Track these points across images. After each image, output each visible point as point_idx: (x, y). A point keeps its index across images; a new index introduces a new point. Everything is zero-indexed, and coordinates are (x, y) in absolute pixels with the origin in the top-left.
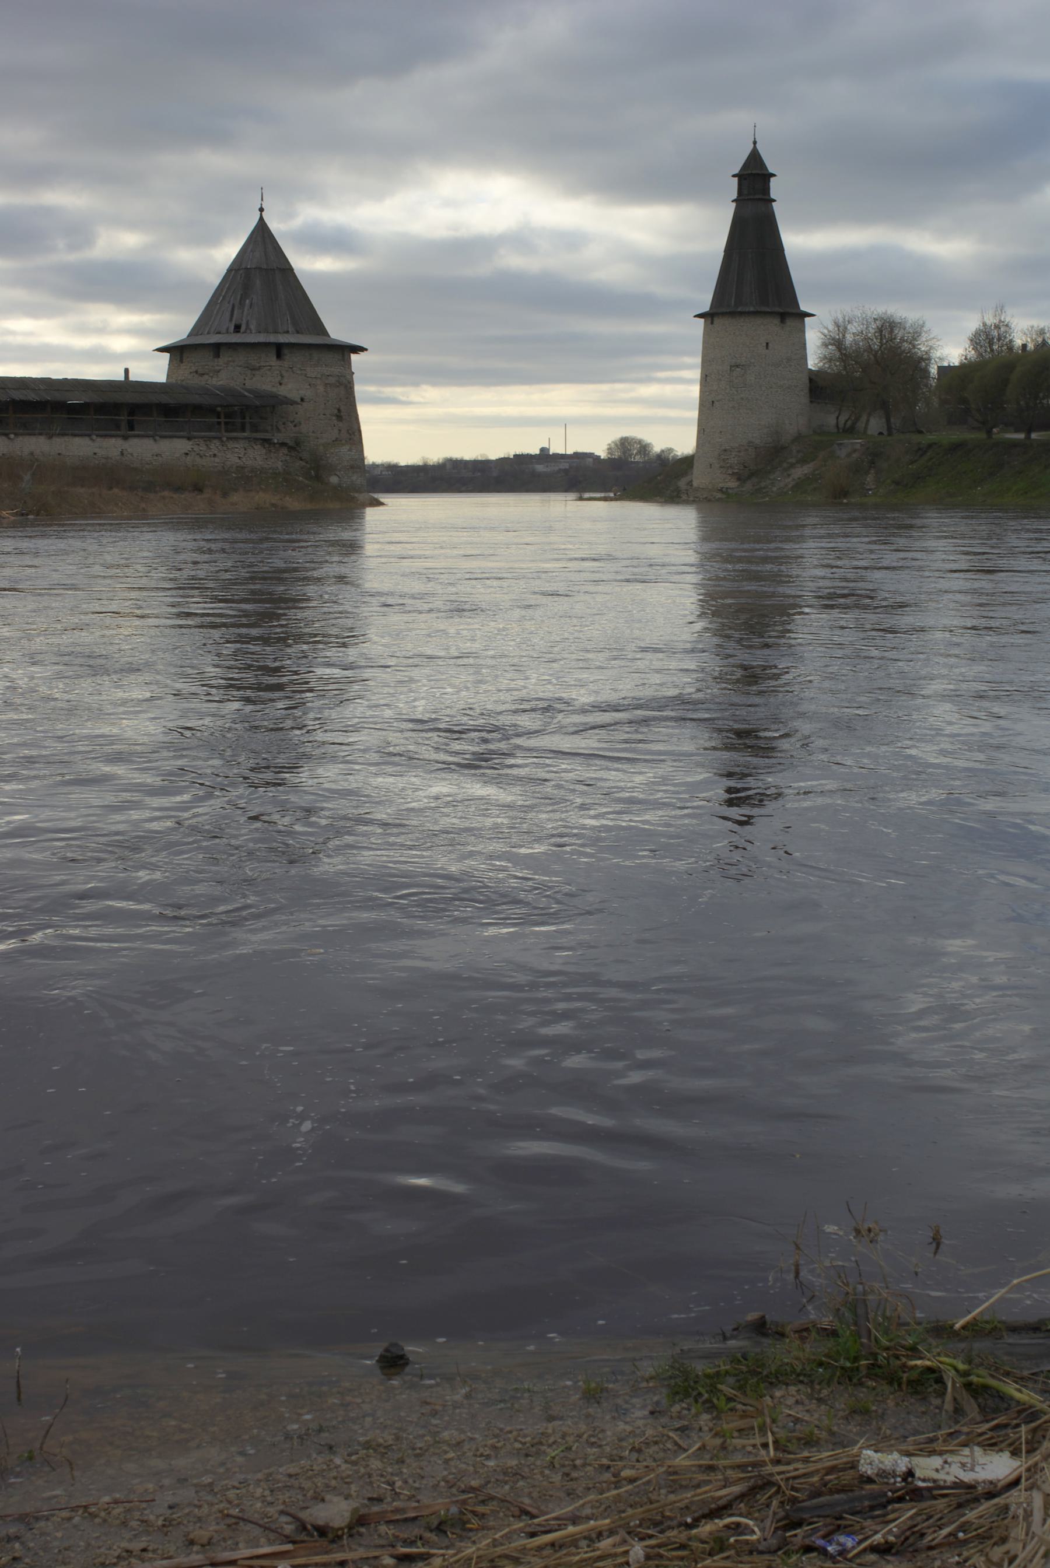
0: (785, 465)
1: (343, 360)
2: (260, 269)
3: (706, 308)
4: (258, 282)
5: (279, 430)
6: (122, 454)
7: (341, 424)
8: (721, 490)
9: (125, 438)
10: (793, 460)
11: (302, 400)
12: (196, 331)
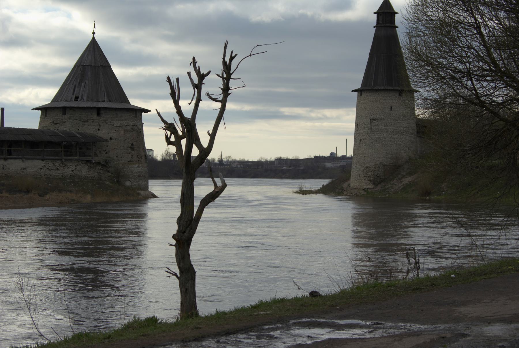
0: (400, 176)
1: (136, 117)
2: (91, 66)
3: (359, 86)
4: (89, 73)
5: (96, 155)
6: (3, 168)
7: (133, 152)
8: (364, 190)
9: (6, 159)
10: (404, 174)
11: (111, 139)
12: (56, 99)
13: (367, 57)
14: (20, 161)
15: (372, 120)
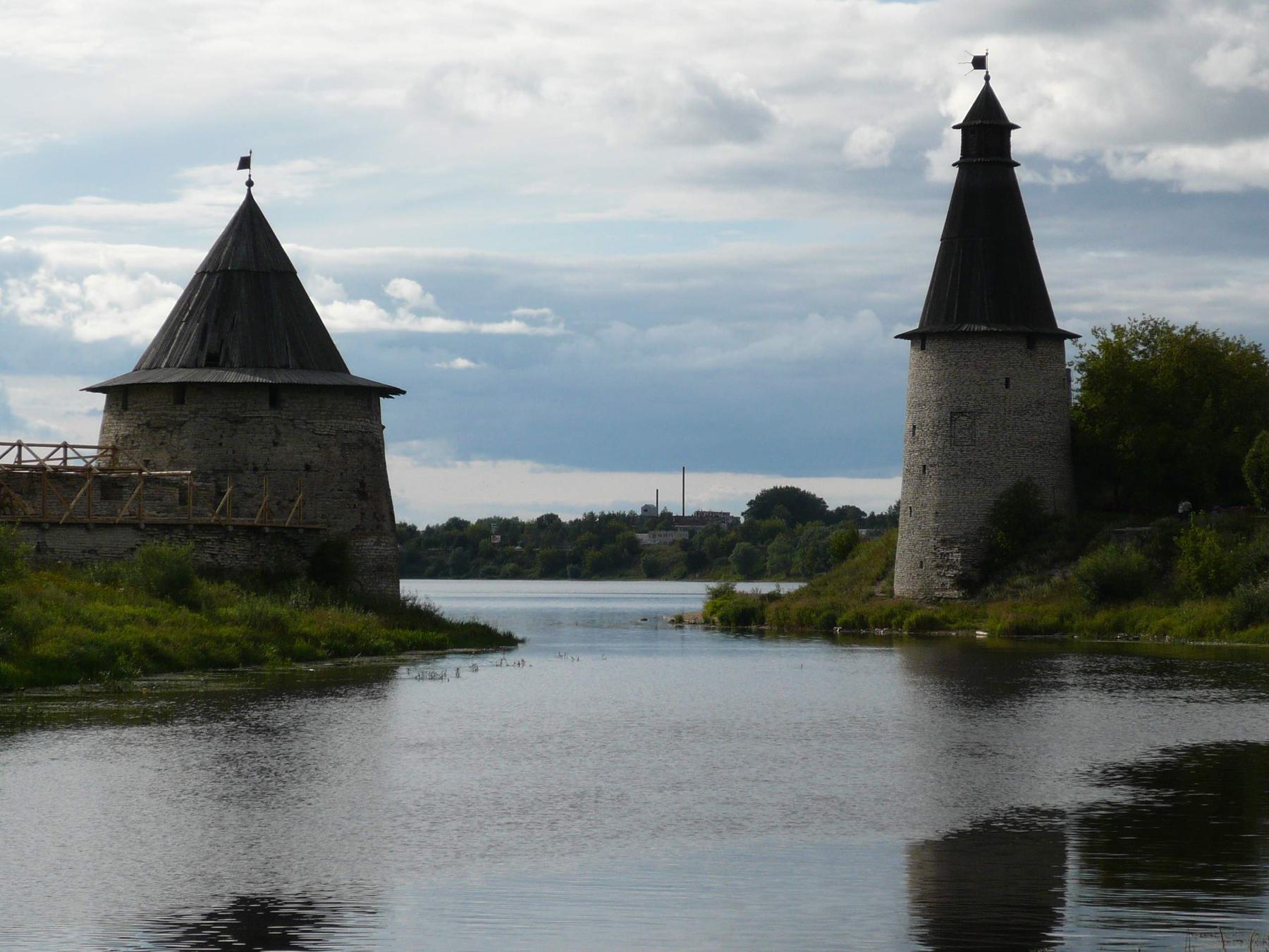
11: (308, 468)
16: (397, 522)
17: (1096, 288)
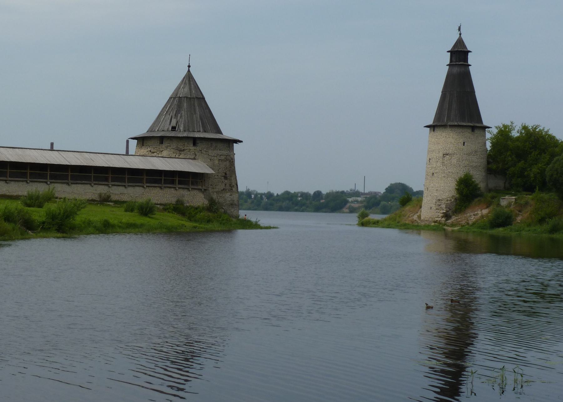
1: (229, 147)
2: (187, 97)
7: (226, 181)
13: (440, 94)
14: (123, 188)
15: (445, 155)
16: (242, 188)
17: (502, 107)
